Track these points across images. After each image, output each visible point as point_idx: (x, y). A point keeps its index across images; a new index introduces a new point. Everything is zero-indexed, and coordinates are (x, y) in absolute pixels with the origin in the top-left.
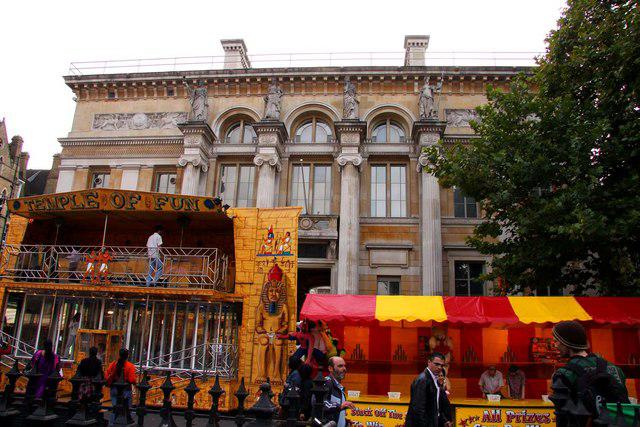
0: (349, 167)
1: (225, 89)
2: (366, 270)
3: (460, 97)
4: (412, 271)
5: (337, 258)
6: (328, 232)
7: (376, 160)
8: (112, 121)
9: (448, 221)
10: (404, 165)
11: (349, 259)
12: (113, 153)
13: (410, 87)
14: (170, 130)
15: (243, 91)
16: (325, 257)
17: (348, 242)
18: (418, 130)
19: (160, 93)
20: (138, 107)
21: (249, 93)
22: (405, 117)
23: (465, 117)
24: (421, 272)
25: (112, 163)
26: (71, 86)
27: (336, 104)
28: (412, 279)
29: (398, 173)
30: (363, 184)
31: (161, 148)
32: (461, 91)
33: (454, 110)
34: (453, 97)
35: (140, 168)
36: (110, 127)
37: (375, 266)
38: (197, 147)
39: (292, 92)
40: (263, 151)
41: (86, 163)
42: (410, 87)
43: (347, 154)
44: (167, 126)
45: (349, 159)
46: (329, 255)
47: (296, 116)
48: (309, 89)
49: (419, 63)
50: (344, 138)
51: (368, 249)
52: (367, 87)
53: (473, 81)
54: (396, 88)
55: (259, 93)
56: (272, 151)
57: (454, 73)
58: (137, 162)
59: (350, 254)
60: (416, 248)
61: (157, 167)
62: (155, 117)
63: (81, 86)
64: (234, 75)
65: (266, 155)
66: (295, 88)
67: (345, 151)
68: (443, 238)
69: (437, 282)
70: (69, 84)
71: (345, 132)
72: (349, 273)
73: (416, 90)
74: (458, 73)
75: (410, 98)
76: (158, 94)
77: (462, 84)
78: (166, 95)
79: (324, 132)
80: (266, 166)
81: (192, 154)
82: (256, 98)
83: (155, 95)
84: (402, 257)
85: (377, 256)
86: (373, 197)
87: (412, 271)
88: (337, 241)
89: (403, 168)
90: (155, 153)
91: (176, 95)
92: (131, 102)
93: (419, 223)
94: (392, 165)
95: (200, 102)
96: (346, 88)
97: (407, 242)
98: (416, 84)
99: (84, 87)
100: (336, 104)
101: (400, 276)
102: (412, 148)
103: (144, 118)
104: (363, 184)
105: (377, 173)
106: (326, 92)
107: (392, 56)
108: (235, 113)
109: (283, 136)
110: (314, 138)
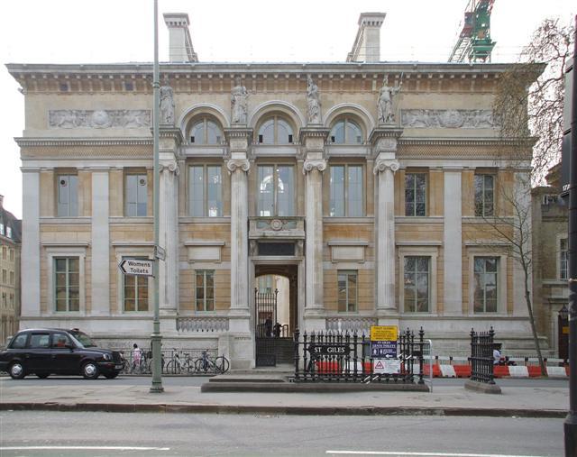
0: (315, 171)
1: (186, 85)
2: (185, 265)
3: (416, 96)
4: (367, 265)
5: (304, 255)
6: (296, 233)
7: (262, 161)
8: (69, 117)
9: (400, 221)
10: (361, 165)
11: (316, 256)
12: (456, 154)
13: (369, 85)
14: (136, 130)
15: (205, 87)
16: (293, 254)
17: (313, 244)
18: (377, 136)
19: (118, 87)
20: (100, 103)
21: (211, 89)
22: (363, 118)
23: (419, 117)
24: (377, 267)
25: (79, 165)
26: (16, 76)
27: (297, 103)
28: (368, 272)
29: (354, 173)
30: (252, 185)
31: (129, 149)
32: (418, 89)
33: (410, 111)
34: (409, 95)
35: (109, 170)
36: (422, 125)
37: (335, 262)
38: (170, 151)
39: (254, 89)
40: (235, 156)
41: (51, 164)
42: (369, 85)
43: (314, 160)
44: (129, 126)
45: (315, 164)
46: (297, 252)
47: (259, 116)
48: (271, 87)
49: (372, 61)
50: (233, 144)
51: (187, 246)
52: (426, 85)
53: (463, 79)
54: (355, 86)
55: (222, 90)
56: (242, 156)
57: (412, 71)
58: (106, 164)
59: (317, 251)
60: (371, 245)
61: (126, 169)
62: (116, 116)
63: (27, 76)
64: (361, 71)
65: (238, 161)
66: (257, 85)
67: (383, 156)
68: (396, 236)
69: (391, 276)
70: (11, 73)
71: (311, 137)
72: (317, 269)
73: (374, 89)
74: (416, 71)
75: (368, 97)
76: (116, 88)
77: (418, 82)
78: (124, 90)
79: (284, 130)
80: (238, 171)
81: (167, 159)
82: (218, 96)
83: (113, 90)
84: (359, 253)
85: (337, 253)
86: (332, 197)
87: (367, 265)
88: (304, 241)
89: (359, 168)
90: (122, 154)
91: (135, 90)
92: (86, 97)
93: (374, 223)
94: (349, 165)
95: (167, 102)
96: (309, 89)
97: (363, 241)
98: (375, 82)
99: (33, 79)
100: (297, 103)
101: (357, 270)
102: (369, 151)
103: (104, 115)
104: (252, 185)
105: (197, 173)
106: (276, 91)
107: (333, 49)
108: (198, 112)
109: (179, 141)
110: (276, 139)
